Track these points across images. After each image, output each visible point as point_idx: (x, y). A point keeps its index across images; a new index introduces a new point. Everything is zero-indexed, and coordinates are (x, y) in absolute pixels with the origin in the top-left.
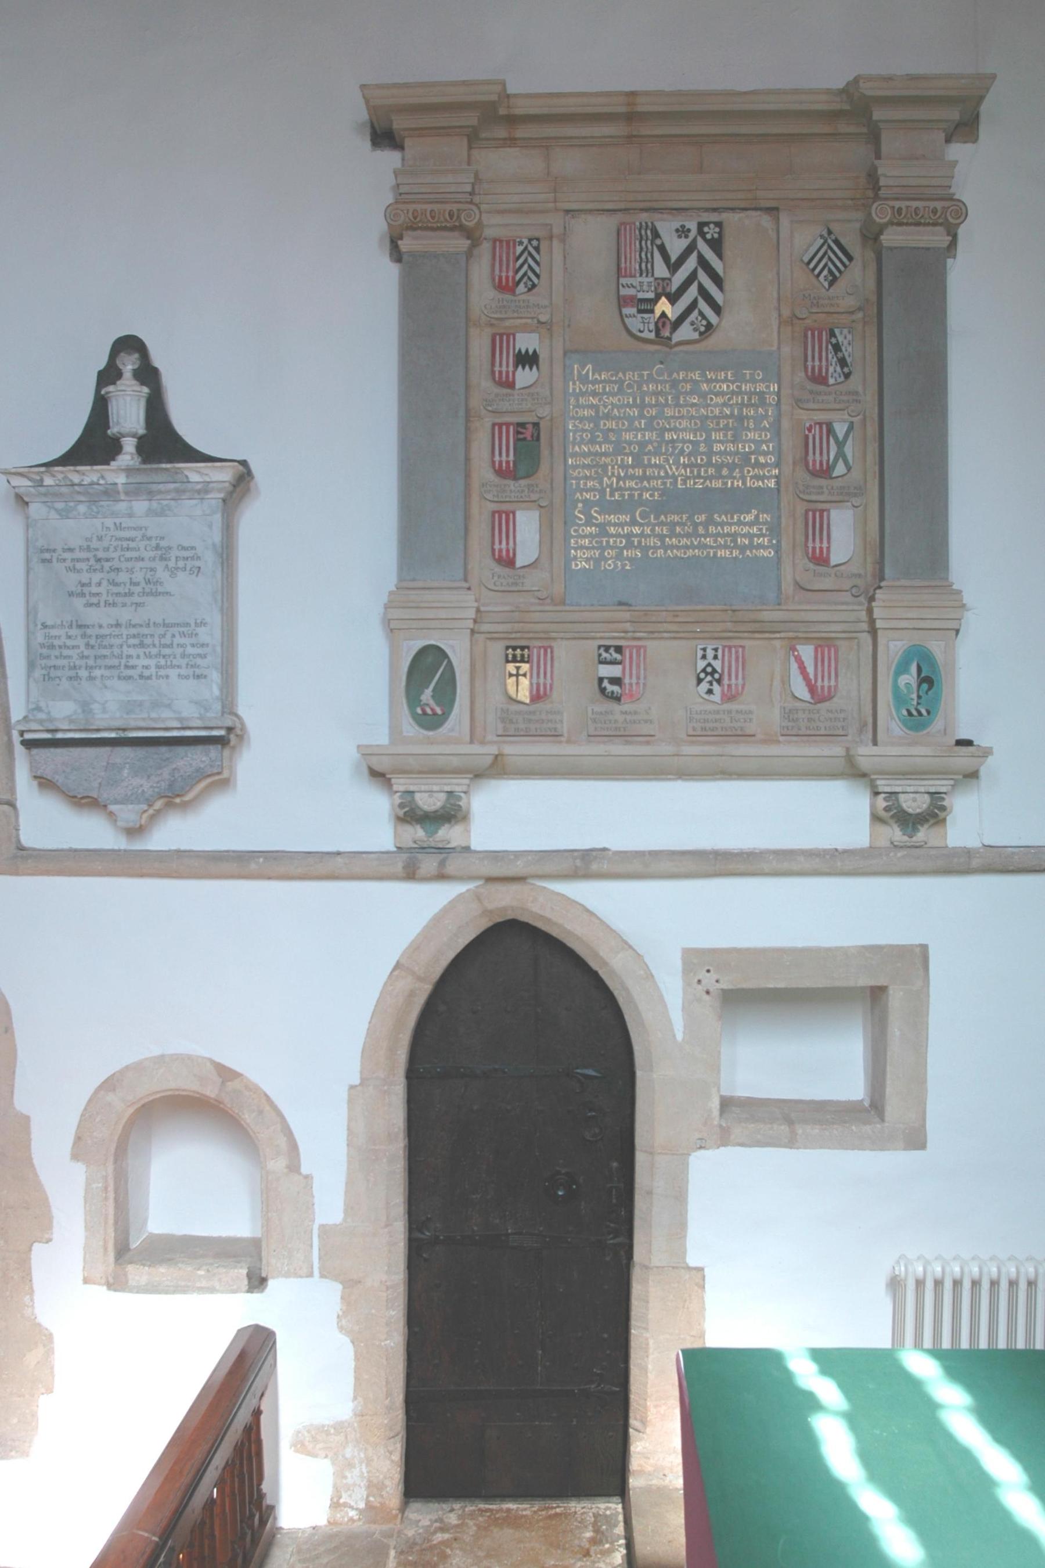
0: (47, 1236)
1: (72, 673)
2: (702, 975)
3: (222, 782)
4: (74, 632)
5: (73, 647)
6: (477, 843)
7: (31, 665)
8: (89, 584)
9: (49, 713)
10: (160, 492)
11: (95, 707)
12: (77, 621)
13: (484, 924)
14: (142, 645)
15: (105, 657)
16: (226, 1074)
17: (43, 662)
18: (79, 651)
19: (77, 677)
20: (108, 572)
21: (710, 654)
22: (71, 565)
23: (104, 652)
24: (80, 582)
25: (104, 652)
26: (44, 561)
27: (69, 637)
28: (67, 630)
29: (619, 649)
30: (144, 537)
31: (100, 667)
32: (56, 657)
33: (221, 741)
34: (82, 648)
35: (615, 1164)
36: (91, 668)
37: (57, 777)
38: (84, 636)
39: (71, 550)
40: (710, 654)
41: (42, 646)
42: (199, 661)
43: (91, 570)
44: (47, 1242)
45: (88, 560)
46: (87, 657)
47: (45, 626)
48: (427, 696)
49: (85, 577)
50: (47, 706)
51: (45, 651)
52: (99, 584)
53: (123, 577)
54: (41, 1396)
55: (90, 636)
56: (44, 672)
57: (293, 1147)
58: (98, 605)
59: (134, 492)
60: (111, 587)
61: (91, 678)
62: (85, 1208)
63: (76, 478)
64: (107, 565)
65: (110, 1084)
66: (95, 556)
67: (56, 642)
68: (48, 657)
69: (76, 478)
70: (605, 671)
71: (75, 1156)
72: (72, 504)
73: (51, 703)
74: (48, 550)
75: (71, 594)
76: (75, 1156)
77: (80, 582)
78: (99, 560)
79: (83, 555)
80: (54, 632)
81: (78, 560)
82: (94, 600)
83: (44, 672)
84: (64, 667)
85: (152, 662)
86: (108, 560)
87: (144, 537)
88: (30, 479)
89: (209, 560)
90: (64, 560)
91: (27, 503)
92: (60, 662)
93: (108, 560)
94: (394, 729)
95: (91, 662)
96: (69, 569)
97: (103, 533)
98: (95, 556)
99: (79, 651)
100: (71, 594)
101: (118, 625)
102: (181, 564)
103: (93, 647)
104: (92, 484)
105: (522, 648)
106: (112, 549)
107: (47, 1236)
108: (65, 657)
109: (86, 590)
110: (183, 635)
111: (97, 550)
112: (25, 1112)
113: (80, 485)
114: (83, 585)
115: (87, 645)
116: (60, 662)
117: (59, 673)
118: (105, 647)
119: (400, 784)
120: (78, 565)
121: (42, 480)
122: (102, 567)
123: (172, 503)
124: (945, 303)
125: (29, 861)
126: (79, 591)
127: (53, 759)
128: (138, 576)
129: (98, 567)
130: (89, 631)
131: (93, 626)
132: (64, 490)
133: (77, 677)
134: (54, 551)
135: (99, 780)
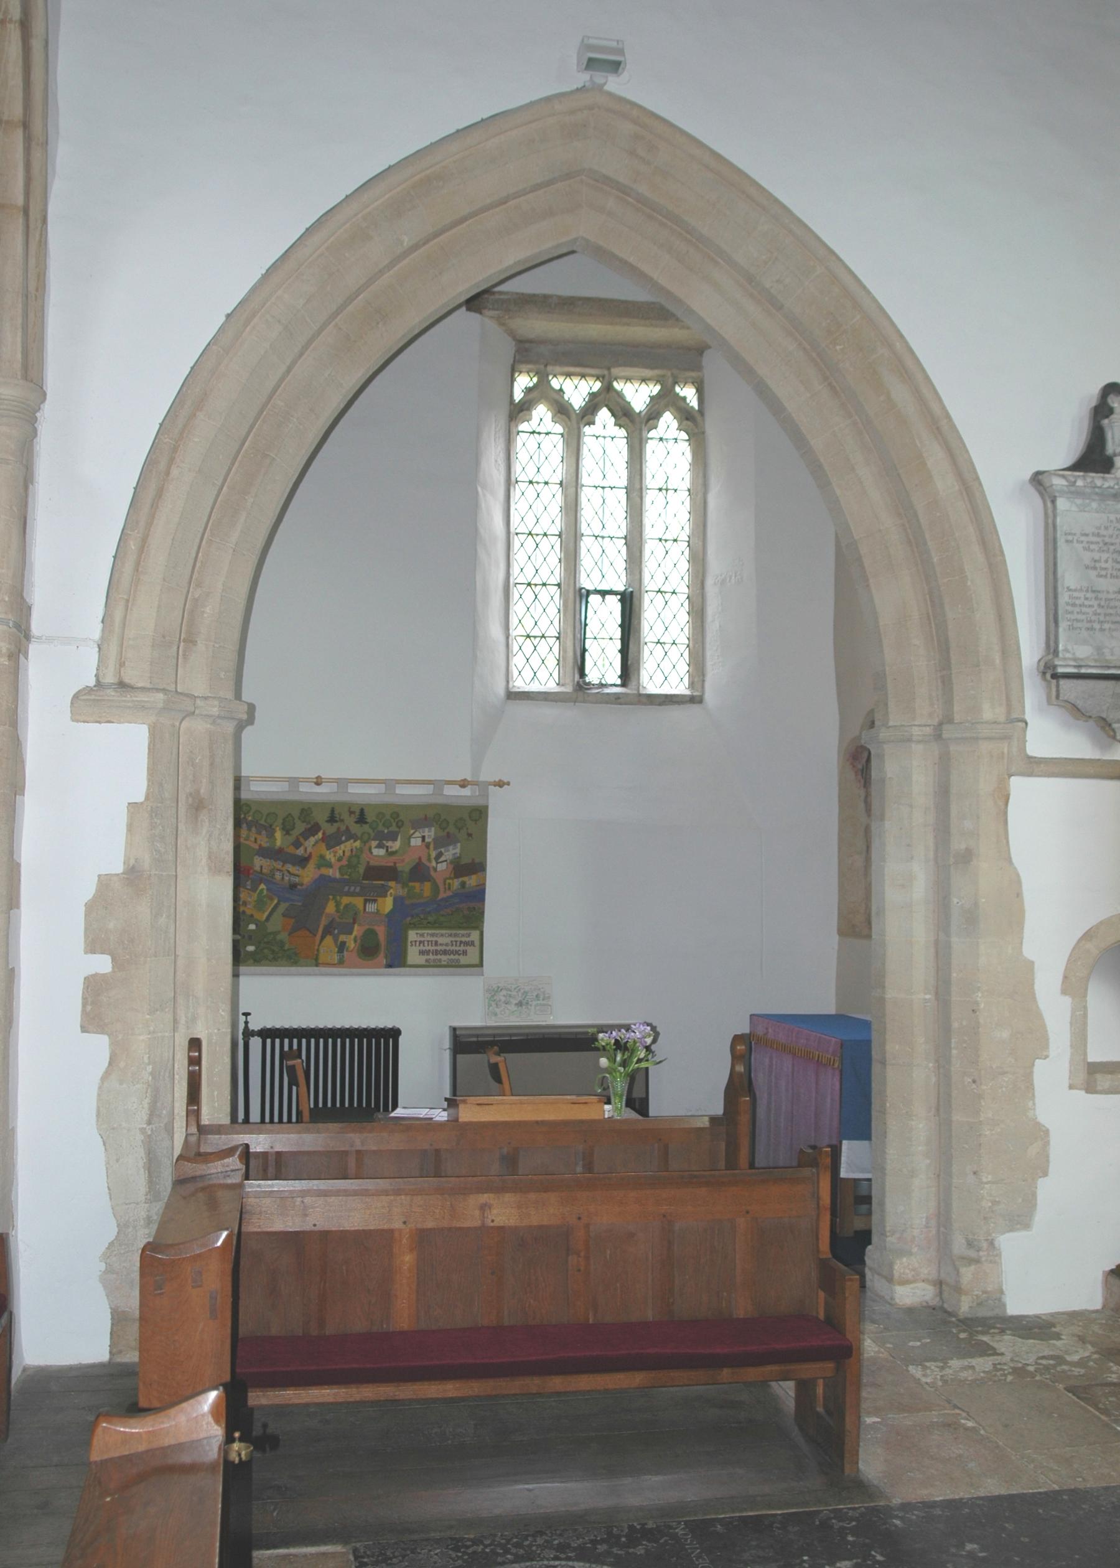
0: (1045, 1053)
1: (1089, 625)
4: (1089, 595)
5: (1090, 606)
8: (1099, 561)
9: (1074, 654)
11: (1106, 651)
12: (1092, 587)
15: (1111, 614)
17: (1069, 616)
18: (1093, 609)
20: (1113, 553)
22: (1087, 546)
23: (1111, 611)
24: (1093, 559)
25: (1111, 611)
26: (1067, 541)
27: (1086, 599)
28: (1085, 593)
31: (1108, 622)
32: (1078, 613)
34: (1096, 607)
36: (1102, 622)
37: (1078, 702)
38: (1096, 598)
39: (1087, 535)
41: (1068, 604)
43: (1101, 551)
44: (1045, 1059)
45: (1098, 543)
46: (1099, 614)
47: (1069, 589)
49: (1097, 556)
50: (1073, 649)
51: (1069, 608)
52: (1106, 561)
54: (1040, 1179)
55: (1101, 599)
56: (1069, 623)
58: (1106, 576)
60: (1114, 564)
61: (1102, 630)
62: (1071, 1030)
63: (1099, 483)
64: (1112, 548)
66: (1103, 541)
67: (1078, 602)
68: (1072, 613)
69: (1099, 483)
72: (1088, 501)
73: (1075, 647)
74: (1070, 534)
75: (1087, 567)
76: (1064, 992)
77: (1093, 559)
78: (1106, 544)
79: (1095, 539)
80: (1076, 594)
81: (1092, 543)
82: (1103, 573)
83: (1069, 623)
84: (1083, 621)
86: (1112, 544)
88: (1067, 481)
90: (1082, 542)
92: (1080, 617)
93: (1112, 544)
95: (1102, 618)
96: (1085, 549)
97: (1109, 524)
98: (1103, 541)
99: (1093, 609)
100: (1087, 567)
103: (1103, 607)
104: (1109, 487)
106: (1114, 536)
107: (1045, 1053)
108: (1084, 614)
109: (1098, 565)
111: (1104, 536)
112: (1031, 959)
113: (1100, 487)
114: (1095, 561)
115: (1099, 605)
116: (1080, 617)
117: (1079, 625)
118: (1111, 608)
120: (1092, 547)
121: (1075, 482)
122: (1109, 549)
125: (1042, 765)
126: (1092, 565)
129: (1105, 548)
130: (1100, 596)
131: (1103, 591)
132: (1088, 490)
133: (1092, 629)
134: (1075, 534)
135: (1108, 705)
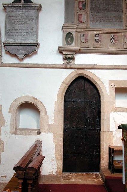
2: (112, 84)
3: (35, 52)
6: (76, 63)
7: (6, 34)
10: (27, 8)
13: (77, 76)
14: (24, 31)
16: (35, 99)
19: (13, 36)
21: (113, 36)
29: (98, 35)
30: (25, 15)
33: (36, 46)
35: (97, 116)
40: (113, 36)
41: (8, 31)
42: (33, 33)
48: (69, 40)
53: (21, 21)
57: (46, 111)
59: (23, 8)
65: (15, 100)
70: (96, 38)
71: (9, 112)
76: (9, 112)
85: (26, 33)
87: (25, 15)
89: (35, 18)
91: (6, 9)
94: (63, 44)
96: (12, 19)
101: (20, 28)
102: (30, 19)
105: (83, 34)
110: (30, 29)
116: (10, 33)
119: (64, 53)
123: (29, 10)
124: (100, 126)
127: (9, 48)
128: (24, 21)
133: (13, 36)
